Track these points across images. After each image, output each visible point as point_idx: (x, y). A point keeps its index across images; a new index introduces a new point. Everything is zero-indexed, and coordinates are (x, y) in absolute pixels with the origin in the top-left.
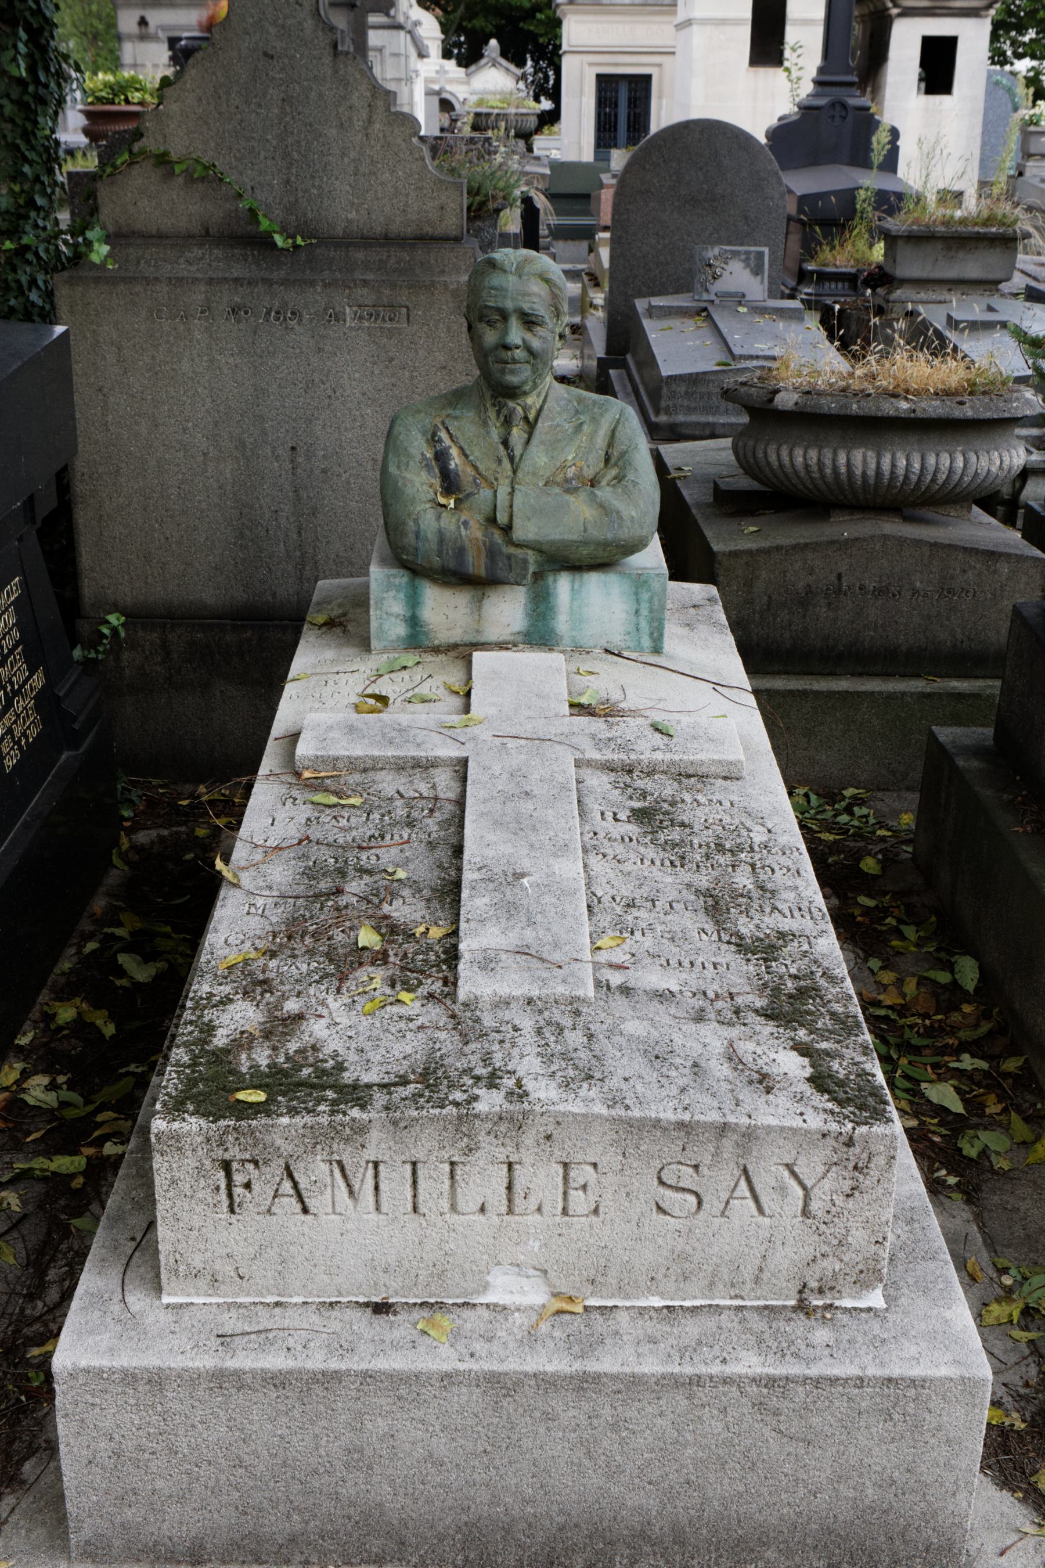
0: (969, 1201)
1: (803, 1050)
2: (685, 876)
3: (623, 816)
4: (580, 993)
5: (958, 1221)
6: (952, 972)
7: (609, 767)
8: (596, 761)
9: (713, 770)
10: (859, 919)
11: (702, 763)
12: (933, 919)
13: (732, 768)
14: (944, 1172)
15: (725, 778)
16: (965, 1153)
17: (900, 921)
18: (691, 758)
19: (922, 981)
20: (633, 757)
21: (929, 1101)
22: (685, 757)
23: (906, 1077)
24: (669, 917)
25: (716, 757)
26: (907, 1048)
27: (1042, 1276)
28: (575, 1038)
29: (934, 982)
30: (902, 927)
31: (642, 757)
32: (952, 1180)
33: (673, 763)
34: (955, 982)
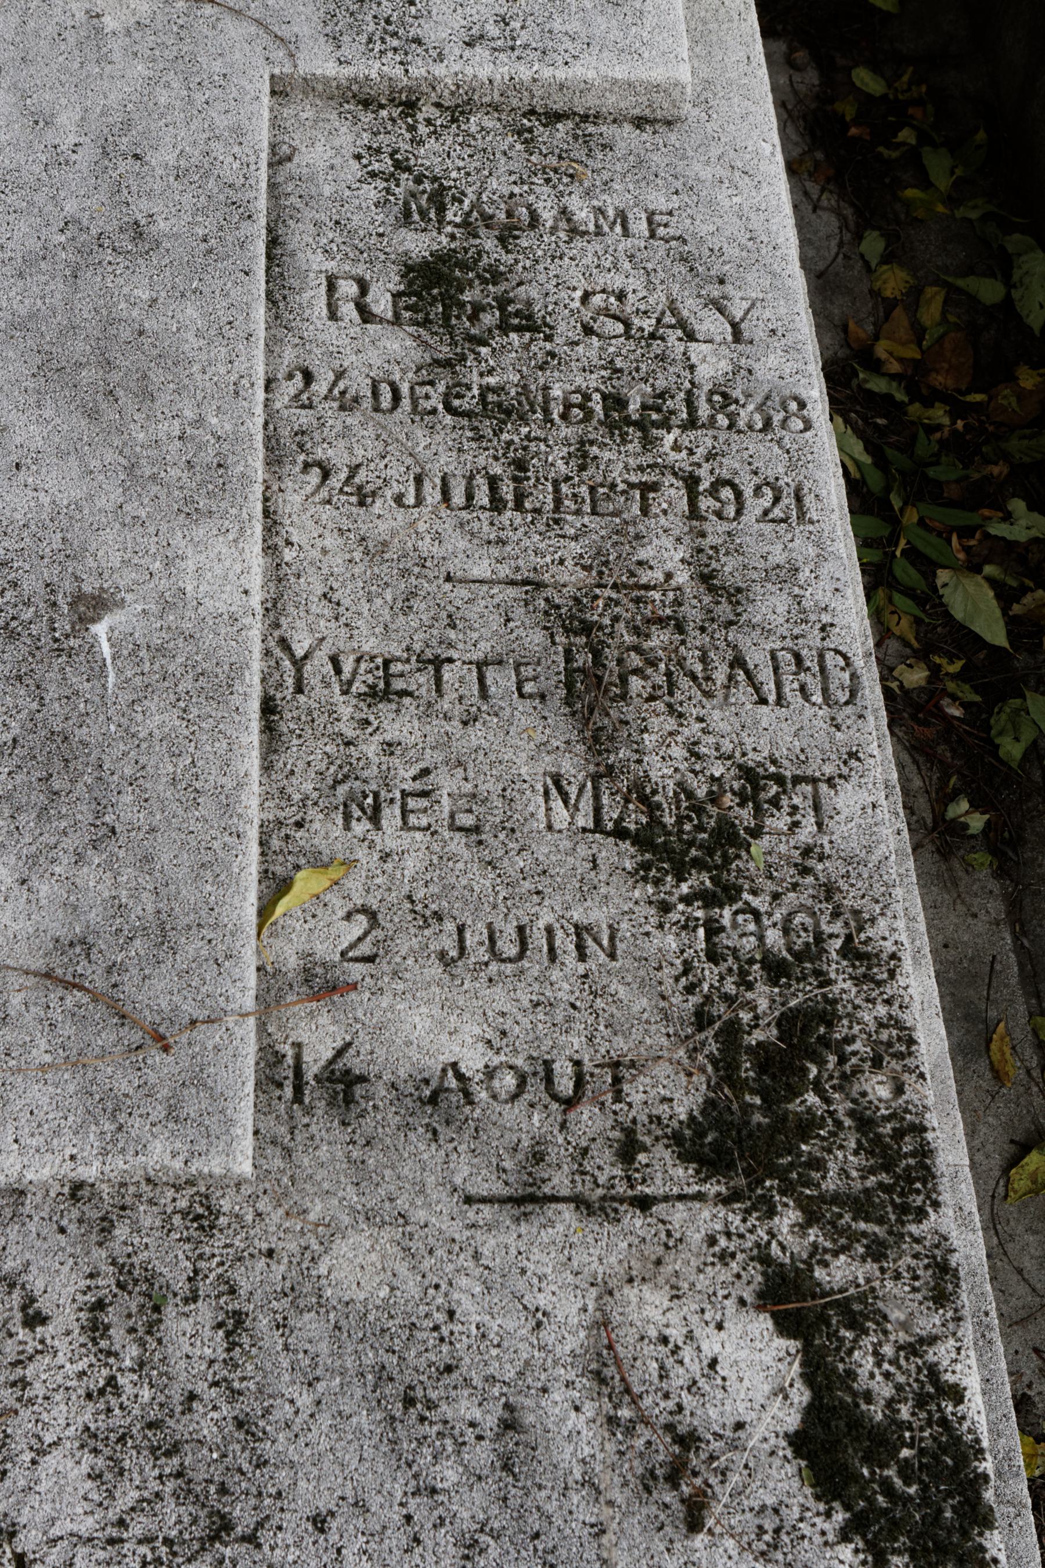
0: (1000, 873)
1: (788, 1299)
2: (531, 547)
3: (381, 303)
4: (215, 1165)
5: (980, 926)
6: (1009, 285)
7: (362, 99)
8: (326, 80)
9: (611, 102)
10: (853, 131)
11: (587, 86)
12: (981, 136)
13: (658, 98)
14: (964, 805)
15: (640, 122)
16: (1001, 753)
17: (923, 138)
18: (561, 74)
19: (954, 297)
20: (418, 70)
21: (947, 615)
22: (547, 73)
23: (913, 554)
24: (476, 735)
25: (620, 72)
26: (921, 488)
27: (1040, 593)
28: (190, 1337)
29: (973, 299)
30: (926, 150)
31: (439, 70)
32: (977, 822)
33: (514, 84)
34: (1008, 303)
